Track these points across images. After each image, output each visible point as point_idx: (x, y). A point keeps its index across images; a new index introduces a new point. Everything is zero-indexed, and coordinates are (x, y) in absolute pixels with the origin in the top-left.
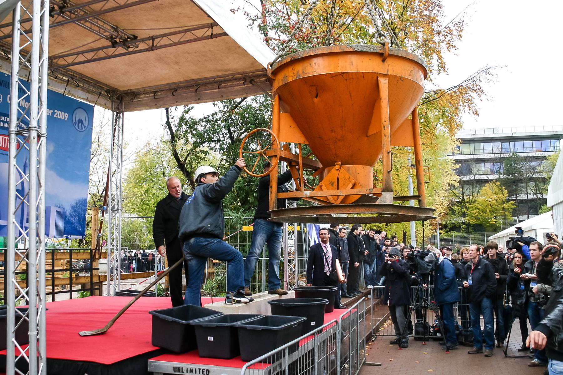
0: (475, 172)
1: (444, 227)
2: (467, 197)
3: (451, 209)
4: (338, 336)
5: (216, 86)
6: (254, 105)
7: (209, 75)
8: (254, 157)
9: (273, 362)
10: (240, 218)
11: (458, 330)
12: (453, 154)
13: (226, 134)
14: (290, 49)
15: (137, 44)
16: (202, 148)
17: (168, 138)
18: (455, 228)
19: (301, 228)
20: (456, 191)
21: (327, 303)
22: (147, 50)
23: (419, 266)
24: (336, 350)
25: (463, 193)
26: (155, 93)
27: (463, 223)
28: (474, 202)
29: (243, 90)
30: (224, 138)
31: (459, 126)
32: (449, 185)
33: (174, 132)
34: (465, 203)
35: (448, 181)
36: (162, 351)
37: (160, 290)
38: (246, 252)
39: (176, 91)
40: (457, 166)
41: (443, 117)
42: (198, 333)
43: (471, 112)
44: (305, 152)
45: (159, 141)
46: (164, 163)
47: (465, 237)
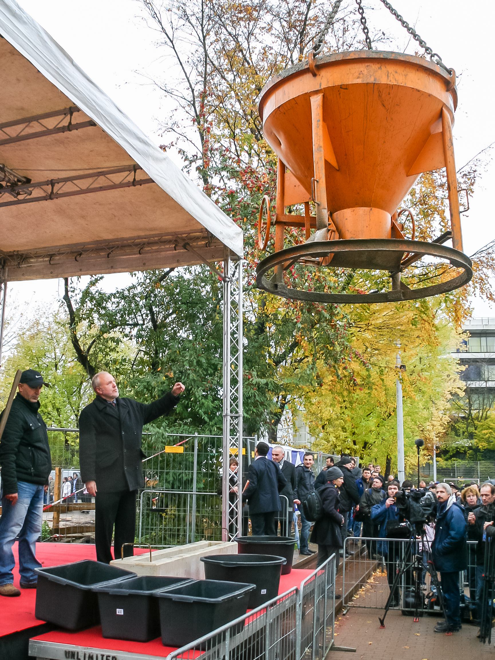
0: (486, 376)
1: (443, 453)
2: (475, 412)
3: (452, 427)
4: (299, 611)
5: (137, 250)
6: (187, 276)
7: (126, 235)
8: (184, 349)
9: (209, 648)
10: (163, 435)
11: (463, 601)
12: (458, 351)
13: (147, 315)
14: (239, 202)
15: (30, 189)
16: (112, 335)
17: (64, 316)
18: (459, 454)
19: (246, 450)
20: (461, 403)
21: (285, 564)
22: (45, 198)
23: (412, 510)
24: (295, 630)
25: (470, 405)
26: (51, 256)
27: (470, 448)
28: (486, 418)
29: (174, 257)
30: (144, 321)
31: (468, 313)
32: (451, 394)
33: (75, 310)
34: (472, 419)
35: (450, 389)
36: (49, 627)
37: (46, 531)
38: (169, 482)
39: (81, 254)
40: (463, 368)
41: (446, 301)
42: (102, 604)
43: (484, 297)
44: (256, 344)
45: (51, 319)
46: (57, 351)
47: (471, 467)
